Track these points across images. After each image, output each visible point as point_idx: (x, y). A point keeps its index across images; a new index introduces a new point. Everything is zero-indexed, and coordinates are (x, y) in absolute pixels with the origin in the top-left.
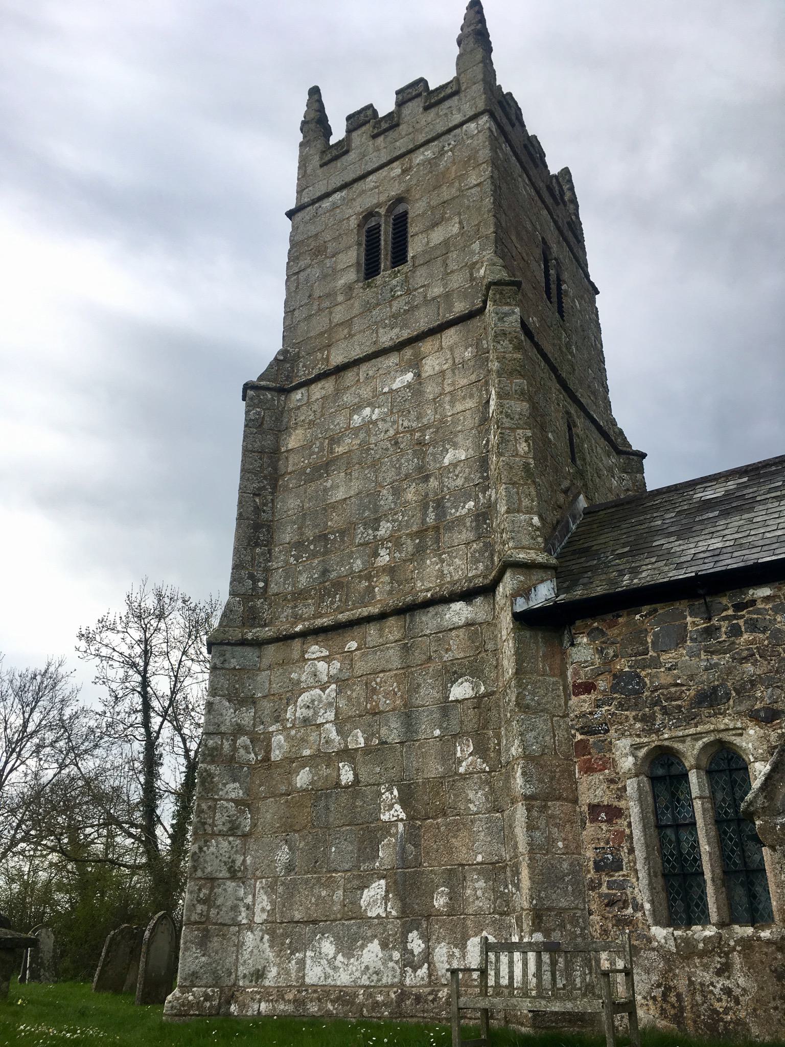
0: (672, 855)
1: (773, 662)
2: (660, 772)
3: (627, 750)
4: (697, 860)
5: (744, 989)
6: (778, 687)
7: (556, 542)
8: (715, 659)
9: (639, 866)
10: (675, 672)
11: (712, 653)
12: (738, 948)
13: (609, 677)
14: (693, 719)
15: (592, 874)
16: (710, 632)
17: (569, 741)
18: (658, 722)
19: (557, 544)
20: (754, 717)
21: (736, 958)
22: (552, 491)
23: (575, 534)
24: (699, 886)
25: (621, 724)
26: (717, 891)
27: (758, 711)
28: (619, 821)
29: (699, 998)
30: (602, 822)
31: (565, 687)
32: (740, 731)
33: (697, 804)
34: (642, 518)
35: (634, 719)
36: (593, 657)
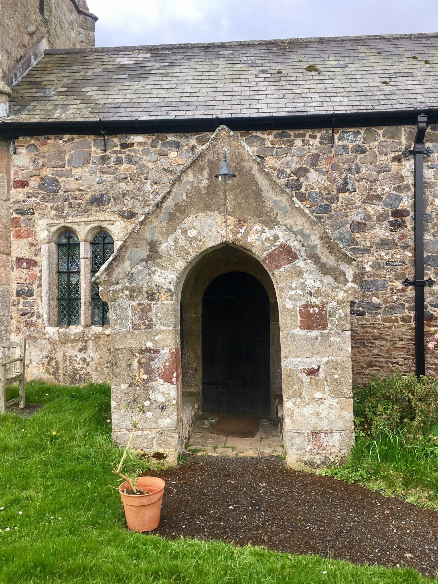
0: (64, 288)
1: (137, 184)
2: (64, 241)
3: (45, 227)
4: (78, 291)
5: (92, 359)
6: (137, 199)
7: (18, 73)
8: (105, 177)
9: (43, 294)
10: (80, 181)
11: (104, 173)
12: (93, 338)
13: (37, 178)
14: (86, 212)
15: (14, 298)
16: (104, 159)
17: (8, 217)
18: (66, 212)
19: (18, 74)
20: (121, 214)
21: (91, 343)
22: (19, 32)
23: (34, 69)
24: (77, 305)
25: (42, 210)
26: (86, 308)
27: (124, 212)
28: (34, 268)
29: (68, 363)
30: (24, 268)
31: (9, 181)
32: (112, 222)
33: (82, 261)
34: (81, 67)
35: (51, 208)
36: (28, 164)
